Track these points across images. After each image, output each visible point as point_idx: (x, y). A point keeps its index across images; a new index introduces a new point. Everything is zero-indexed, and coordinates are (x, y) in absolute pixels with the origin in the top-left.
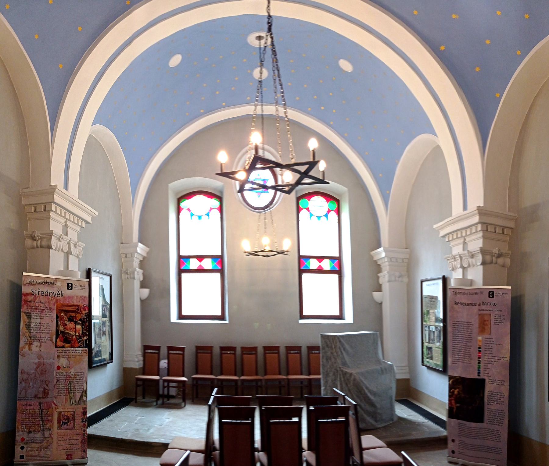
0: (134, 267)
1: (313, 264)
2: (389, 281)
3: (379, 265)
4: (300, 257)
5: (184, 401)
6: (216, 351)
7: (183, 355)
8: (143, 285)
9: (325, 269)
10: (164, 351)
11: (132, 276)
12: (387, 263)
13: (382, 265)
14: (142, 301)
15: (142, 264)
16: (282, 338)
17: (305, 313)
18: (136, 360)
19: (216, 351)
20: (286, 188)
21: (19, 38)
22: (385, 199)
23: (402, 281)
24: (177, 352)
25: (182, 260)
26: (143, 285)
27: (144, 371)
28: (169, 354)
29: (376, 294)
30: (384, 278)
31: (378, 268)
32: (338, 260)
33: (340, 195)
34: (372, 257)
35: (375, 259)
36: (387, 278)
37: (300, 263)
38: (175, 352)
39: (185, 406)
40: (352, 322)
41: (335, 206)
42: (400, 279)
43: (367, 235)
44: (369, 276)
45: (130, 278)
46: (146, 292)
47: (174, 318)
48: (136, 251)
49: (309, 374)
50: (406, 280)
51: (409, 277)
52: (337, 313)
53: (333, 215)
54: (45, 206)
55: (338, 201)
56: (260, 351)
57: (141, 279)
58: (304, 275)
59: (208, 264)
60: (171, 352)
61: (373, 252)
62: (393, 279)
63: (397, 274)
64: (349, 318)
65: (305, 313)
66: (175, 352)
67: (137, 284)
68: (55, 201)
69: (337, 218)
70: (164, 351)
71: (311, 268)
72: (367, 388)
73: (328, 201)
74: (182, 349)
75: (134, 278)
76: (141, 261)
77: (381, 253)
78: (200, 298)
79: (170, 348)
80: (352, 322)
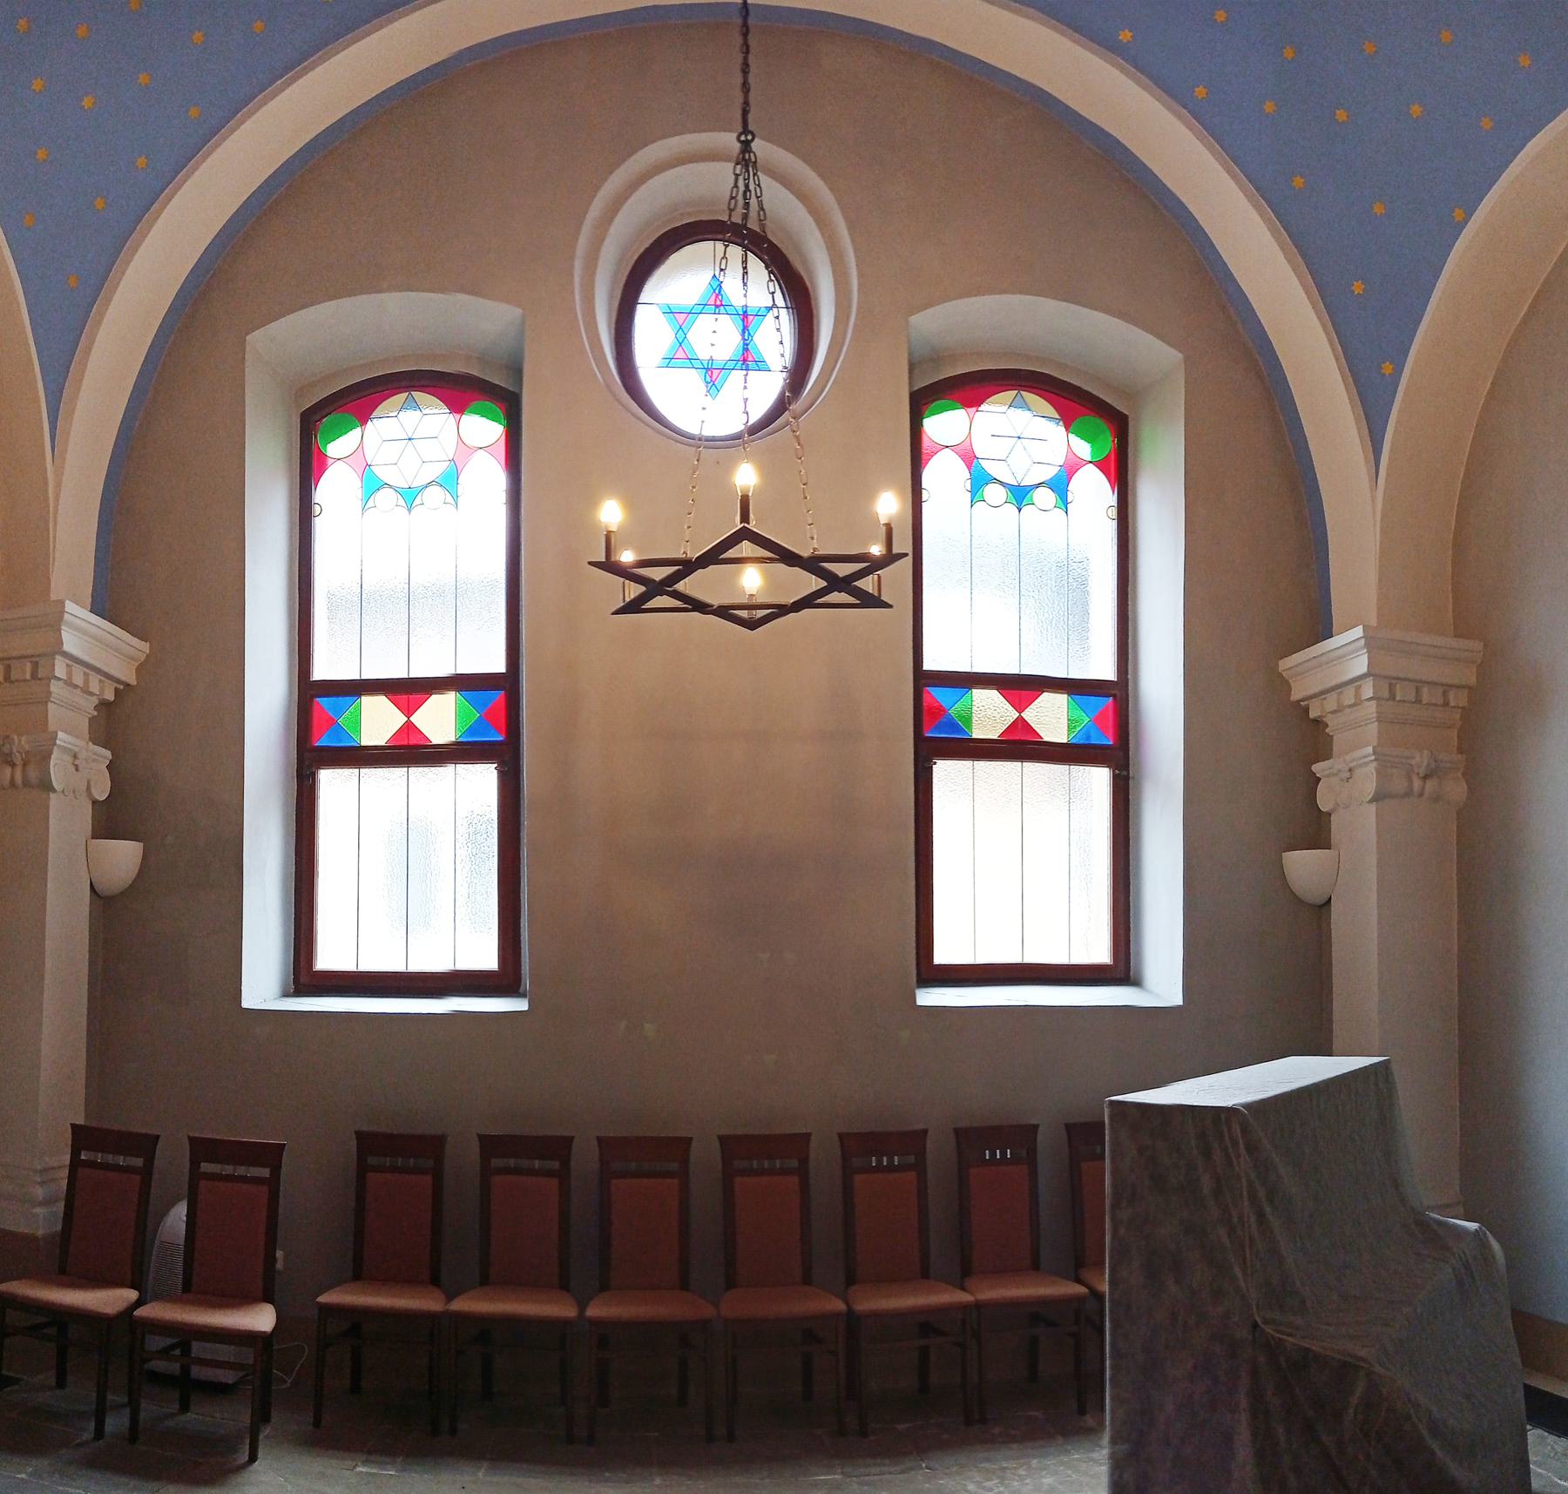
0: (51, 727)
1: (988, 714)
2: (1377, 798)
3: (1319, 723)
4: (924, 679)
5: (262, 1416)
6: (464, 1156)
7: (273, 1183)
8: (110, 821)
9: (1048, 737)
10: (172, 1159)
11: (33, 774)
12: (1371, 708)
13: (1333, 723)
14: (105, 904)
15: (113, 720)
16: (813, 1086)
17: (943, 955)
18: (40, 1192)
19: (464, 1156)
20: (746, 548)
21: (12, 252)
22: (1373, 404)
23: (1437, 798)
24: (241, 1171)
25: (313, 698)
26: (110, 821)
27: (68, 1258)
28: (195, 1176)
29: (1302, 866)
30: (1352, 782)
31: (1308, 737)
32: (1115, 698)
33: (1134, 394)
34: (1284, 685)
35: (1296, 695)
36: (1368, 781)
37: (924, 713)
38: (228, 1169)
39: (253, 1458)
40: (1178, 1000)
41: (1107, 444)
42: (1430, 785)
43: (1261, 579)
44: (1265, 772)
45: (26, 783)
46: (122, 858)
47: (262, 983)
48: (58, 649)
49: (964, 1273)
50: (1457, 790)
51: (1471, 774)
52: (1100, 954)
53: (1094, 490)
54: (35, 665)
55: (1120, 426)
56: (706, 1154)
57: (102, 792)
58: (945, 772)
59: (441, 719)
60: (206, 1167)
61: (1285, 664)
62: (1399, 785)
63: (1421, 760)
64: (1163, 981)
65: (943, 955)
66: (228, 1169)
67: (67, 820)
68: (66, 647)
69: (1111, 499)
70: (172, 1159)
71: (977, 734)
72: (1435, 1429)
73: (1068, 421)
74: (271, 1155)
75: (47, 787)
76: (103, 705)
77: (1347, 654)
78: (403, 884)
79: (203, 1149)
80: (1178, 1000)
